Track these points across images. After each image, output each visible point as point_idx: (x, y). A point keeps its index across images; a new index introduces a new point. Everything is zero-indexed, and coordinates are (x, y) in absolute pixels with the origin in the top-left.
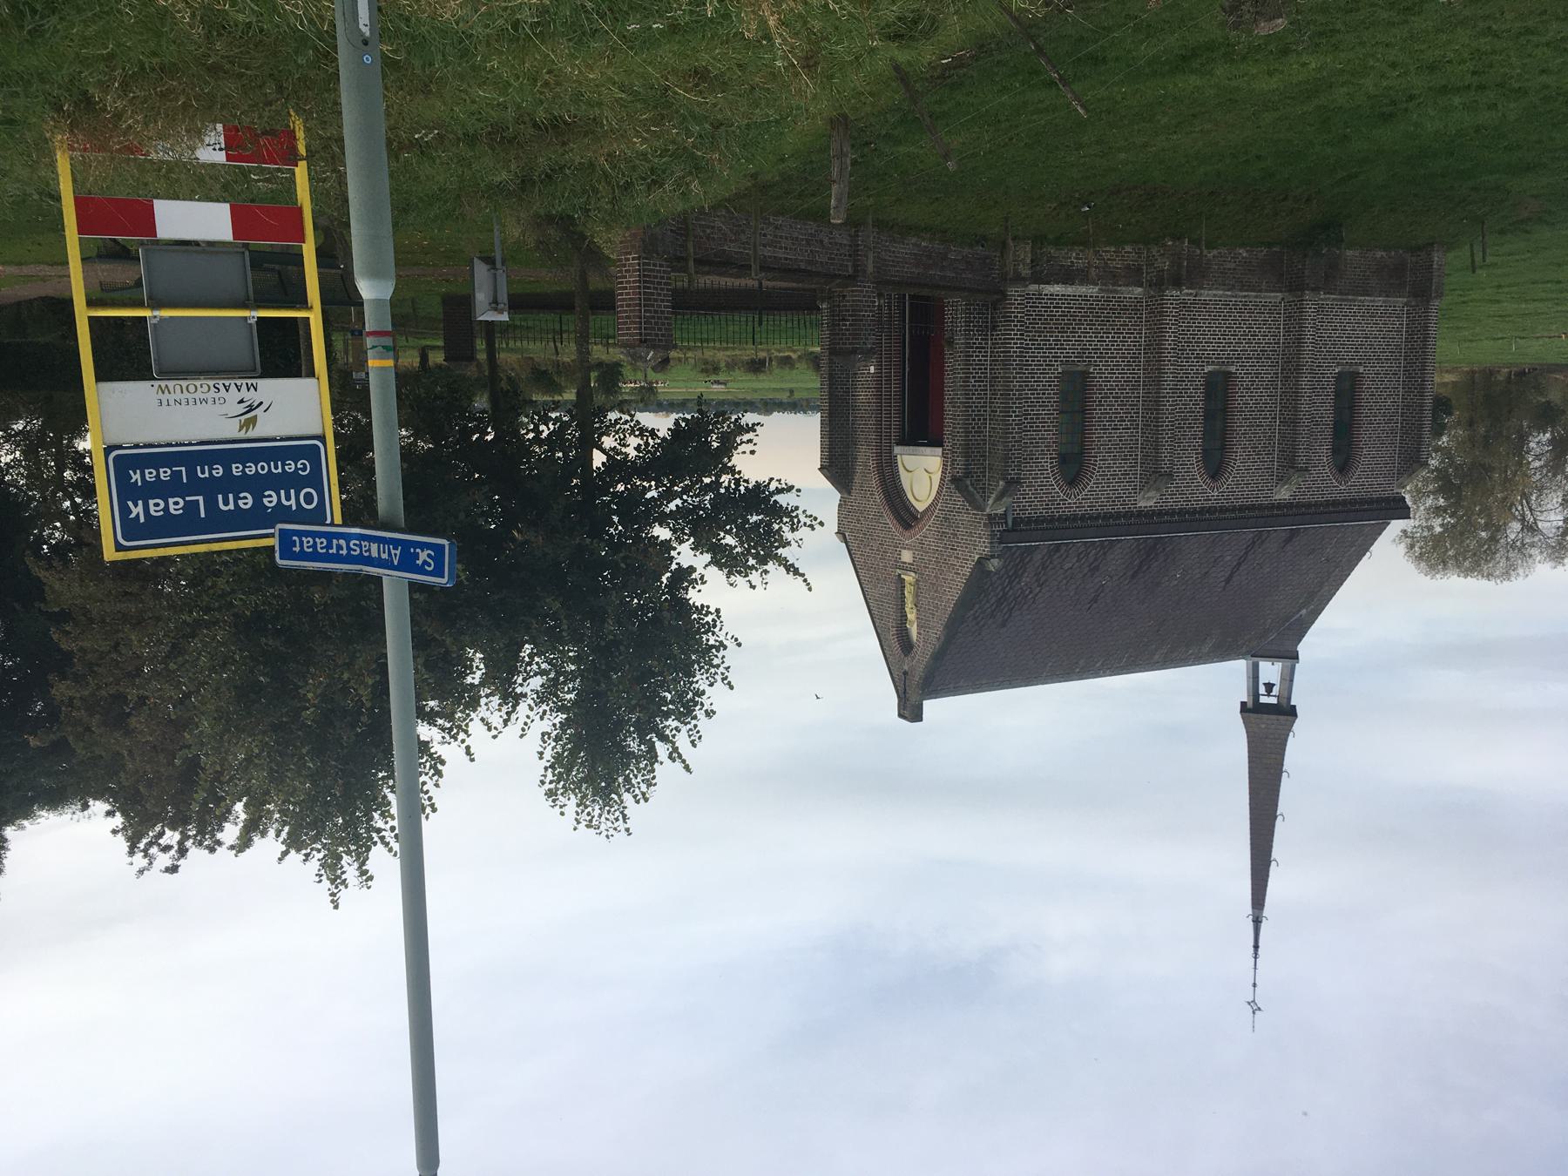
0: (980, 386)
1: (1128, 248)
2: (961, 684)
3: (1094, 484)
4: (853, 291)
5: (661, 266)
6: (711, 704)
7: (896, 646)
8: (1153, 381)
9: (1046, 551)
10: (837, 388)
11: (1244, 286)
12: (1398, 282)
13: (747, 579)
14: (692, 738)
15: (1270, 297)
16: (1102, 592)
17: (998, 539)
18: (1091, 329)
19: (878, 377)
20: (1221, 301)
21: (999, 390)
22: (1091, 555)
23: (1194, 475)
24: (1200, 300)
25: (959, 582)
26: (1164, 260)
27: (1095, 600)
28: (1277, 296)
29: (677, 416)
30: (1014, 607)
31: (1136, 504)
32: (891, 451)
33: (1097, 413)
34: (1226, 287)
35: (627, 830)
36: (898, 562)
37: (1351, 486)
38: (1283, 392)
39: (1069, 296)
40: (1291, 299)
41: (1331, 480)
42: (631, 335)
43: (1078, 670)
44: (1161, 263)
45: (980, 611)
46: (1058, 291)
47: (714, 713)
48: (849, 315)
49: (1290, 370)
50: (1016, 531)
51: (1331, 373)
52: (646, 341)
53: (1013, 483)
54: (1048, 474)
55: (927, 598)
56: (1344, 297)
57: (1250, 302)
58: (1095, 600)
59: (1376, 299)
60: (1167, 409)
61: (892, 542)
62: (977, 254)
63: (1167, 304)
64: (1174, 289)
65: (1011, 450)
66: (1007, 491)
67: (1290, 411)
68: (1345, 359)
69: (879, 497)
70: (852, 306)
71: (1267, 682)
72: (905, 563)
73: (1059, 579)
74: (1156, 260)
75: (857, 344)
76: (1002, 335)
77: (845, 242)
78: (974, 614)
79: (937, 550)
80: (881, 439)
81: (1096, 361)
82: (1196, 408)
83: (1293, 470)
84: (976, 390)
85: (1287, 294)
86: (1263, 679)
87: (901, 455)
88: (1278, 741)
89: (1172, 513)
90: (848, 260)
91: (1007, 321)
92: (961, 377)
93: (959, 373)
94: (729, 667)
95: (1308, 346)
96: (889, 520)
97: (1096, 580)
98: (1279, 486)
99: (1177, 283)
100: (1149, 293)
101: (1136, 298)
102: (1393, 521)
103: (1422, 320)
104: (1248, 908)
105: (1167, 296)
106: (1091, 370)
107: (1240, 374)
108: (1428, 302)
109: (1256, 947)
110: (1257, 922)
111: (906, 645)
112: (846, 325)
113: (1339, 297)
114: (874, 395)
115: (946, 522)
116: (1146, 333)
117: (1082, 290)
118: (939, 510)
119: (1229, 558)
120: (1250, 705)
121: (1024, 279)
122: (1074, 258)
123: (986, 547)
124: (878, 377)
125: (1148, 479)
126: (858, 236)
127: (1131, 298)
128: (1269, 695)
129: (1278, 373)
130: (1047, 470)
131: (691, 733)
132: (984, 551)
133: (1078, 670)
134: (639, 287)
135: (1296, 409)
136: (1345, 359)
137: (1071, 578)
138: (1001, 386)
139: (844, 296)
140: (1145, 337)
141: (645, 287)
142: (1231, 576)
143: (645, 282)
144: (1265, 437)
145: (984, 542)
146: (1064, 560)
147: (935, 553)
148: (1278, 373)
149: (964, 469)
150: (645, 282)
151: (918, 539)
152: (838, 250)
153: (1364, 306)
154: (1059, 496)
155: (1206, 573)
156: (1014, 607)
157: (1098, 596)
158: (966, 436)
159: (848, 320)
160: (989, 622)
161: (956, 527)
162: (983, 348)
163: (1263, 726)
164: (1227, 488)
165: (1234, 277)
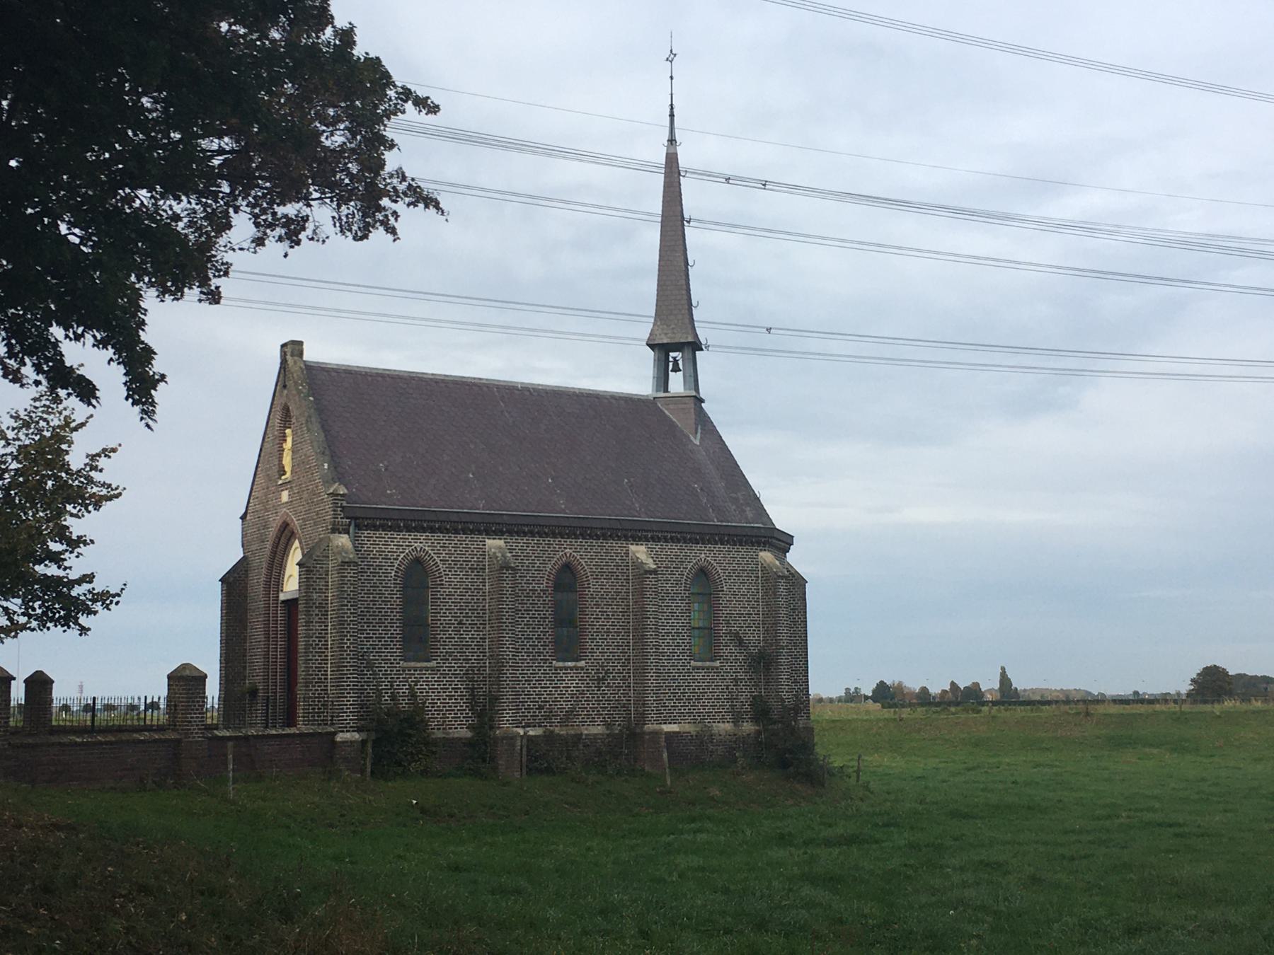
71: (678, 373)
109: (672, 115)
110: (672, 141)
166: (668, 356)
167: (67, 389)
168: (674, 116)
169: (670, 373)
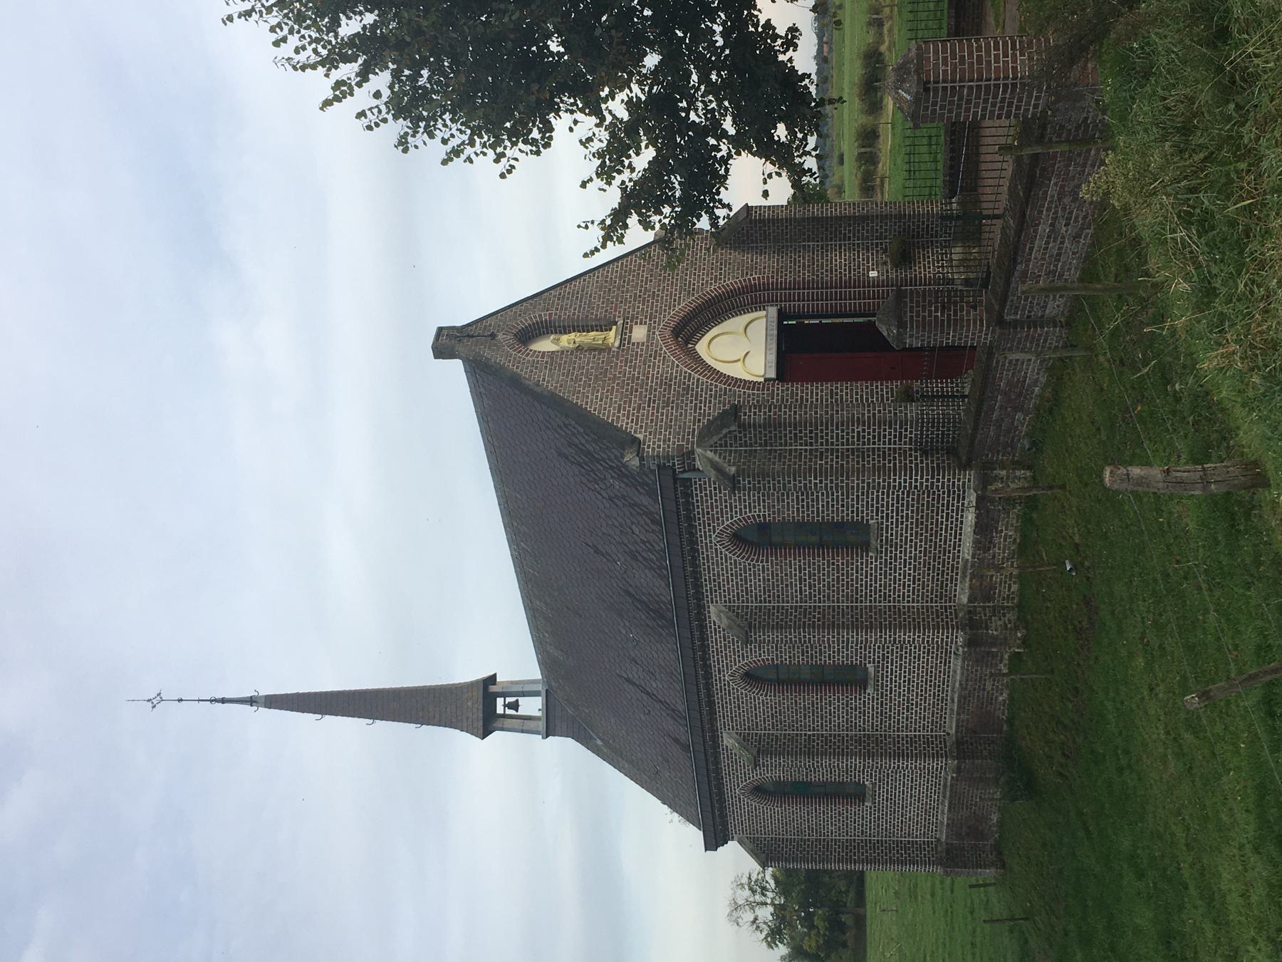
0: (853, 437)
1: (1015, 588)
2: (486, 401)
3: (735, 561)
4: (981, 321)
5: (1036, 106)
6: (416, 147)
7: (524, 322)
8: (857, 619)
9: (653, 510)
10: (850, 225)
11: (965, 698)
12: (963, 833)
13: (594, 176)
14: (368, 113)
15: (951, 722)
16: (608, 560)
17: (664, 464)
18: (920, 552)
19: (864, 282)
20: (949, 677)
22: (651, 555)
23: (747, 657)
24: (950, 657)
25: (609, 411)
26: (999, 629)
27: (597, 551)
28: (951, 729)
29: (814, 77)
30: (583, 467)
31: (712, 602)
32: (771, 301)
33: (819, 561)
34: (963, 683)
35: (230, 18)
36: (632, 321)
37: (740, 799)
38: (843, 737)
39: (961, 529)
40: (948, 744)
41: (746, 781)
42: (936, 65)
43: (515, 524)
44: (996, 625)
45: (576, 431)
46: (967, 517)
47: (405, 150)
48: (949, 316)
49: (869, 745)
50: (675, 483)
51: (864, 778)
52: (927, 90)
53: (734, 483)
54: (746, 513)
55: (588, 365)
56: (948, 789)
57: (946, 704)
58: (597, 551)
59: (945, 816)
60: (824, 637)
61: (656, 311)
62: (1019, 440)
63: (948, 633)
64: (964, 641)
65: (774, 480)
66: (722, 476)
67: (822, 746)
68: (879, 790)
69: (713, 288)
70: (962, 320)
71: (520, 704)
72: (631, 332)
73: (619, 519)
74: (1000, 619)
75: (912, 327)
76: (917, 465)
77: (1047, 311)
78: (570, 425)
79: (648, 378)
80: (785, 289)
81: (881, 558)
82: (825, 657)
83: (755, 753)
84: (848, 434)
85: (954, 739)
86: (522, 700)
87: (766, 316)
88: (454, 720)
89: (703, 638)
90: (1022, 315)
91: (933, 471)
92: (863, 414)
93: (869, 411)
94: (471, 162)
95: (894, 763)
96: (684, 305)
97: (620, 555)
98: (738, 737)
99: (971, 643)
100: (961, 610)
101: (955, 596)
102: (702, 832)
103: (921, 858)
104: (265, 691)
105: (957, 633)
106: (871, 554)
107: (865, 697)
108: (941, 864)
109: (223, 701)
110: (251, 701)
111: (527, 336)
112: (936, 311)
113: (949, 784)
114: (841, 277)
115: (684, 389)
116: (913, 607)
118: (698, 380)
119: (654, 685)
120: (493, 689)
121: (984, 488)
122: (1007, 533)
123: (653, 449)
124: (864, 282)
125: (742, 616)
126: (1055, 326)
127: (955, 590)
128: (505, 706)
129: (864, 731)
130: (750, 512)
131: (375, 111)
133: (515, 524)
134: (1006, 78)
135: (824, 754)
136: (879, 790)
137: (621, 531)
138: (853, 466)
139: (975, 308)
140: (909, 607)
141: (1006, 86)
142: (634, 684)
143: (1014, 86)
144: (793, 721)
145: (659, 447)
146: (642, 526)
147: (644, 375)
148: (864, 731)
149: (749, 423)
150: (1014, 86)
151: (661, 349)
152: (1038, 304)
153: (938, 804)
154: (718, 525)
155: (636, 662)
156: (583, 467)
157: (603, 555)
158: (790, 423)
159: (942, 315)
160: (563, 440)
161: (677, 404)
162: (900, 440)
163: (470, 704)
164: (733, 689)
165: (975, 689)
166: (504, 716)
167: (764, 865)
168: (223, 698)
169: (519, 713)
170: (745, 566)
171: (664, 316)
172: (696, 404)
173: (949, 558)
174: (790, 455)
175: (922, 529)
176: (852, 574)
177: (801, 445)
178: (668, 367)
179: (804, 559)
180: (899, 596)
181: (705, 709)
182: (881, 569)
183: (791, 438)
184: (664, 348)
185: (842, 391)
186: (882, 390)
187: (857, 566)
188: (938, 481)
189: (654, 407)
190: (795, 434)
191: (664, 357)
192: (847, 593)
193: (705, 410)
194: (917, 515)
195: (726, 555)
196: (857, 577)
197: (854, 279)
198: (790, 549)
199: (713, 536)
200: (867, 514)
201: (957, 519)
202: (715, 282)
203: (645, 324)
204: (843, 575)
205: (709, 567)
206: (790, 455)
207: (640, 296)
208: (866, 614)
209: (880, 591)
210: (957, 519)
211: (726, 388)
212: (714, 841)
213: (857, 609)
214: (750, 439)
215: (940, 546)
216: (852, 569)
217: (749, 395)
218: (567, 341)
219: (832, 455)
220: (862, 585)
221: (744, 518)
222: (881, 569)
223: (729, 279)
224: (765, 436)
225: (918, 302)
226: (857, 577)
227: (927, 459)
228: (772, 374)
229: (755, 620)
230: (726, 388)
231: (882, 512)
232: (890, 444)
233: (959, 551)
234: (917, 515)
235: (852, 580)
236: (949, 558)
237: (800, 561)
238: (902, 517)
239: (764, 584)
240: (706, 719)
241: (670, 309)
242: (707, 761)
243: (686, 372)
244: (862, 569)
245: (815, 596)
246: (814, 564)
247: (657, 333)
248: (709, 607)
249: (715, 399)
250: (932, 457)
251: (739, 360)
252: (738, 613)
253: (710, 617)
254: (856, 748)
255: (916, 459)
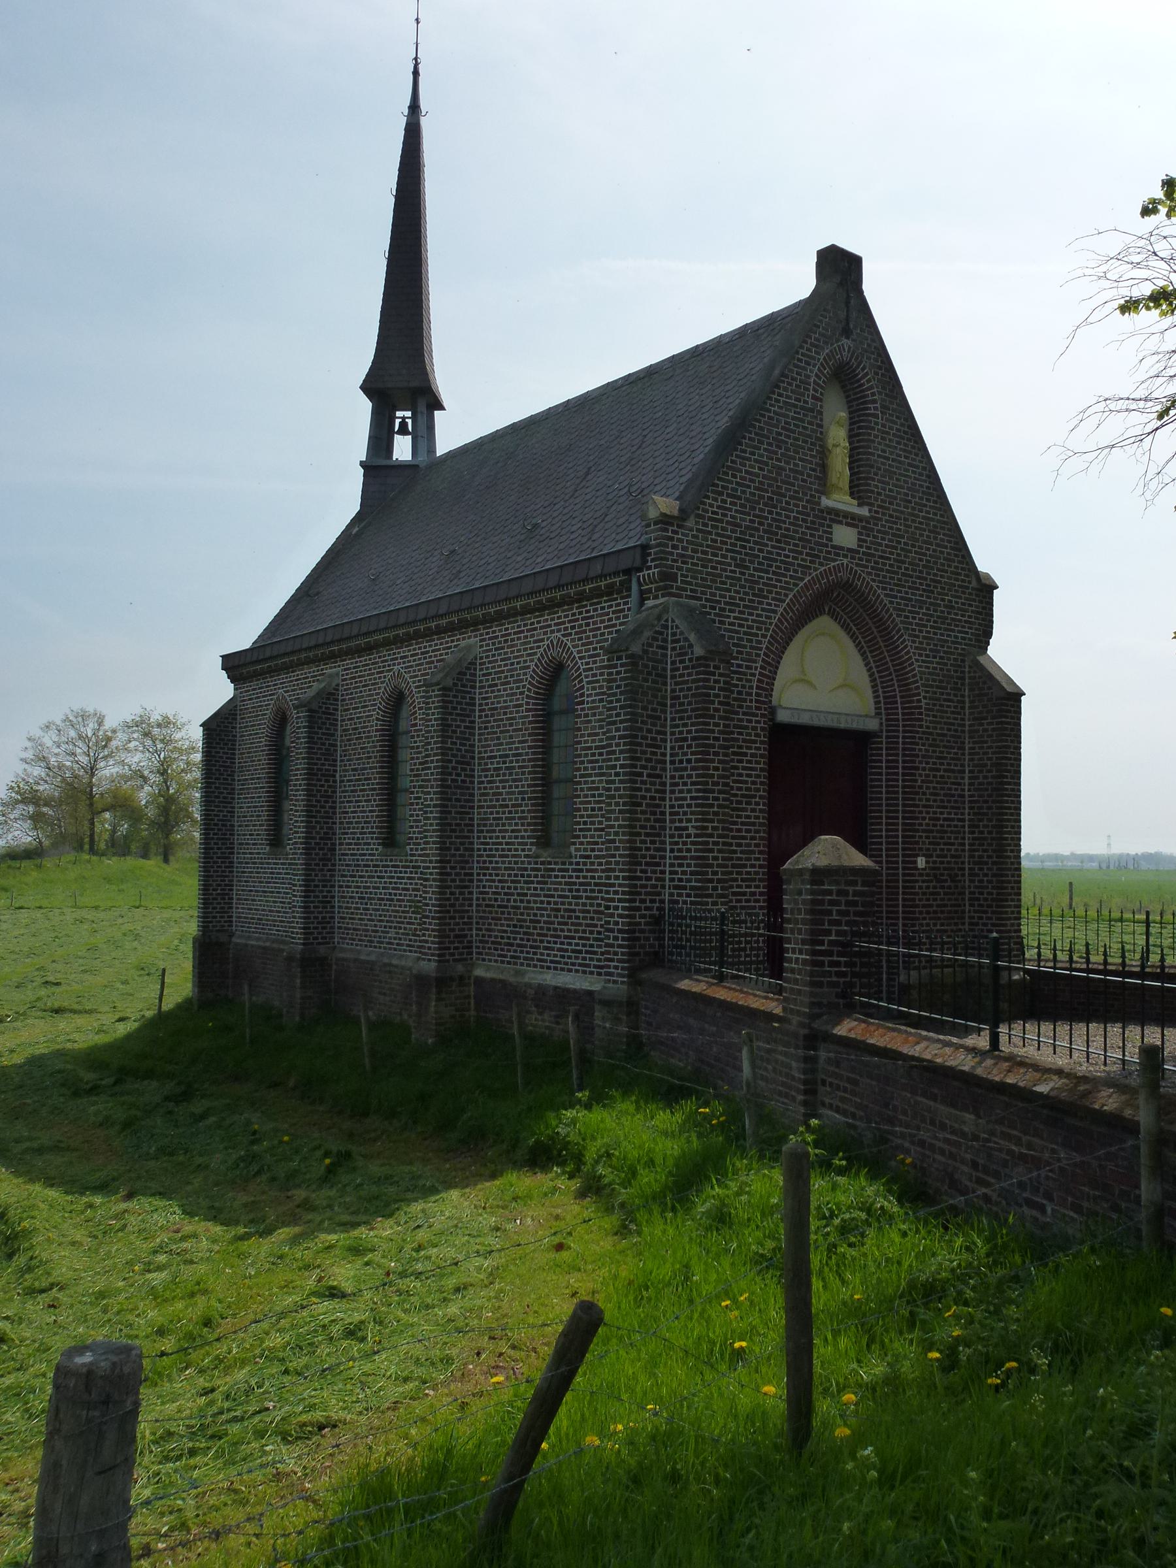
3: (528, 667)
17: (650, 554)
18: (535, 915)
21: (643, 812)
39: (562, 969)
49: (320, 849)
54: (587, 677)
55: (800, 459)
101: (484, 960)
104: (424, 122)
106: (534, 848)
109: (416, 73)
112: (838, 933)
117: (550, 978)
118: (775, 612)
127: (490, 960)
128: (404, 418)
132: (674, 532)
162: (676, 887)
170: (522, 681)
171: (870, 574)
172: (738, 605)
173: (528, 953)
174: (658, 732)
175: (562, 917)
176: (510, 825)
177: (672, 748)
178: (796, 571)
179: (530, 760)
180: (484, 887)
181: (361, 642)
182: (516, 863)
183: (681, 733)
184: (823, 569)
185: (753, 810)
186: (753, 866)
187: (519, 831)
188: (616, 938)
189: (735, 545)
190: (685, 739)
191: (810, 568)
192: (488, 819)
193: (729, 617)
194: (580, 911)
195: (535, 654)
196: (506, 831)
197: (914, 837)
198: (542, 741)
199: (559, 635)
200: (582, 843)
201: (573, 964)
202: (916, 648)
203: (859, 546)
204: (510, 812)
205: (522, 632)
206: (658, 732)
207: (899, 543)
208: (461, 844)
209: (491, 862)
210: (573, 964)
211: (761, 649)
212: (234, 665)
213: (469, 831)
214: (682, 676)
215: (542, 942)
216: (516, 824)
217: (750, 681)
218: (838, 436)
219: (657, 791)
220: (497, 837)
221: (580, 674)
222: (516, 863)
223: (920, 666)
224: (685, 697)
225: (855, 904)
226: (506, 831)
227: (646, 924)
228: (783, 717)
229: (455, 696)
230: (761, 649)
231: (585, 864)
232: (671, 873)
233: (535, 966)
234: (580, 911)
235: (504, 825)
236: (528, 953)
237: (527, 754)
238: (578, 890)
239: (501, 708)
240: (352, 644)
241: (880, 582)
242: (310, 649)
243: (786, 595)
244: (516, 837)
245: (486, 776)
246: (523, 773)
247: (845, 561)
248: (476, 636)
249: (745, 633)
250: (651, 931)
251: (803, 672)
252: (465, 674)
253: (464, 639)
254: (318, 833)
255: (647, 909)
